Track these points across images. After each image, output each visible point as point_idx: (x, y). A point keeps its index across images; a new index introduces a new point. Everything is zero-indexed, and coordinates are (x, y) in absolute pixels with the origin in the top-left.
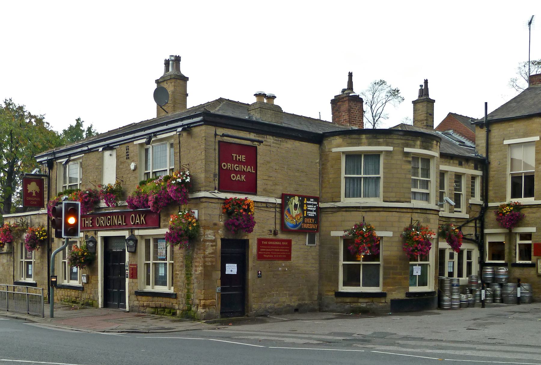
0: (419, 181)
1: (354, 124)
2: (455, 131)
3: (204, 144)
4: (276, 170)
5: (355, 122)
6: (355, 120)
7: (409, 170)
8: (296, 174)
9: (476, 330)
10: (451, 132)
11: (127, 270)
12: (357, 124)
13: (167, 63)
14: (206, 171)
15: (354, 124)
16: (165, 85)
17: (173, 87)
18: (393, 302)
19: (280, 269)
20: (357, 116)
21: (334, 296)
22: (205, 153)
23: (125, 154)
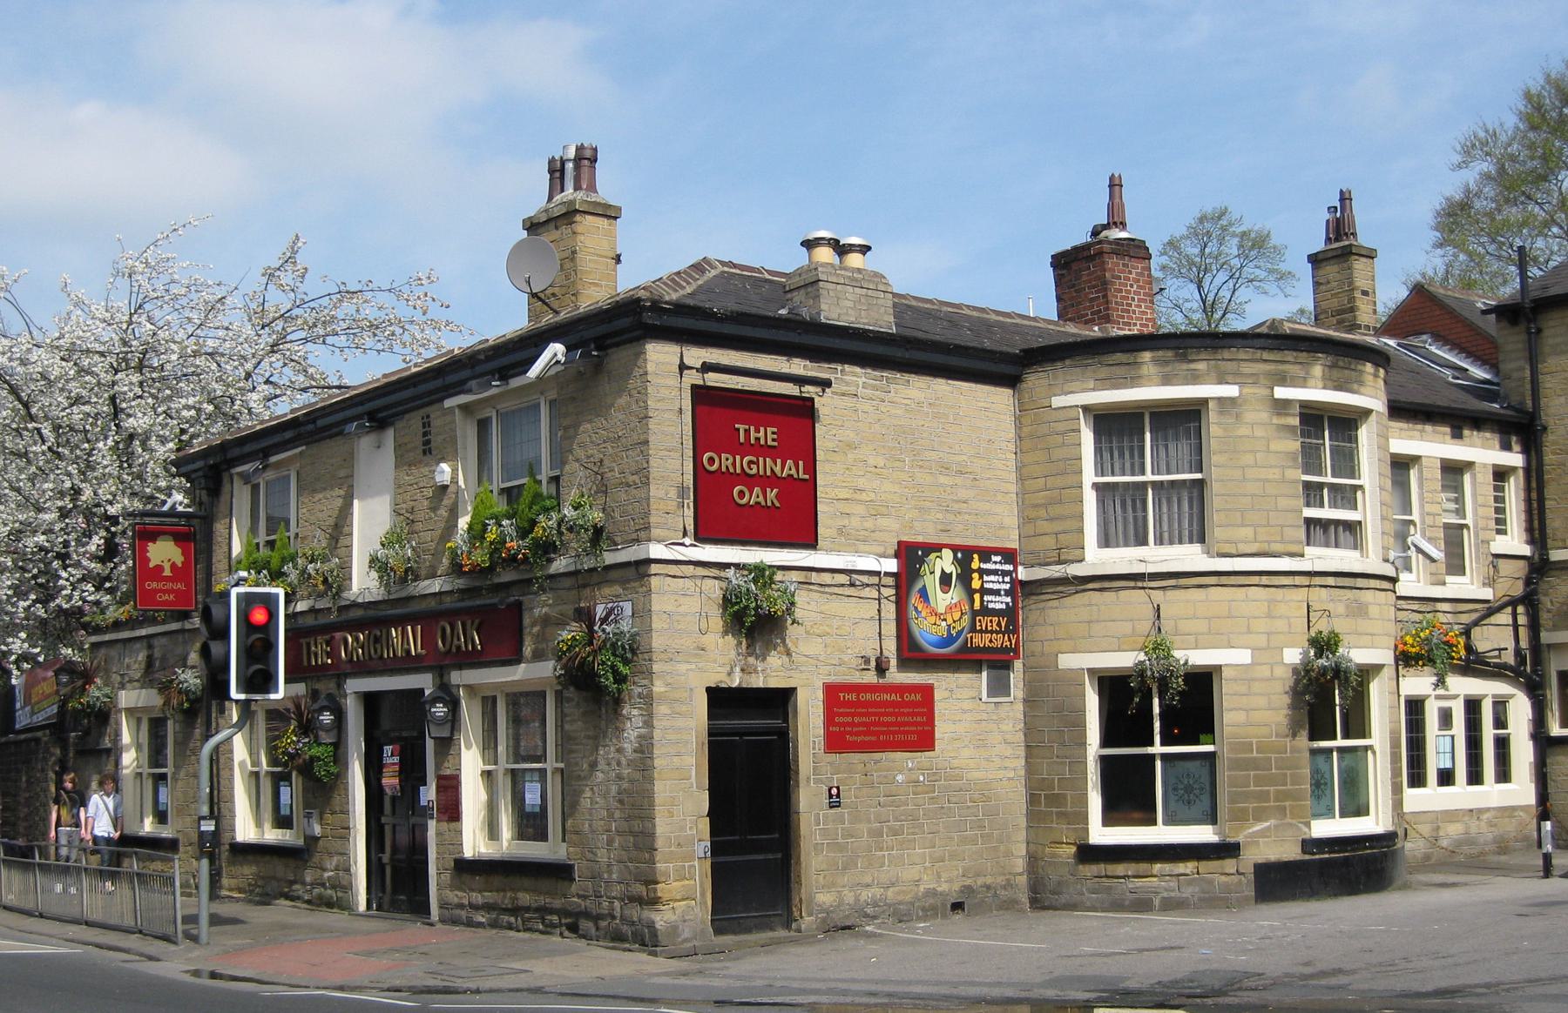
8: (942, 479)
15: (1124, 323)
20: (1133, 299)
23: (419, 440)
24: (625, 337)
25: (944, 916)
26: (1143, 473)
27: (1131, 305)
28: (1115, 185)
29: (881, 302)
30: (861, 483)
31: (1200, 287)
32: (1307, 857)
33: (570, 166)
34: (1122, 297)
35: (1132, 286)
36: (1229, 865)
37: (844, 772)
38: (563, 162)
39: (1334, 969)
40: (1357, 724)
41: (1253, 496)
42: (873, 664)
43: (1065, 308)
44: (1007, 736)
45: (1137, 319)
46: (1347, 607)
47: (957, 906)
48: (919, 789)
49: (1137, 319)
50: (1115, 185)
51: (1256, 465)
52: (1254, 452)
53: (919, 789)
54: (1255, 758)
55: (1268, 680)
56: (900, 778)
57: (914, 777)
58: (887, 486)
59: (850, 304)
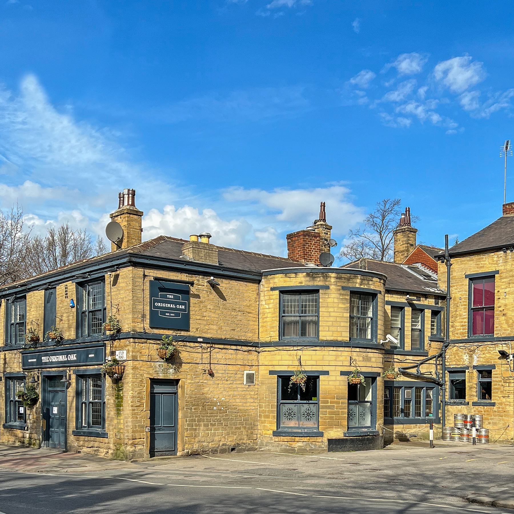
0: (393, 318)
1: (309, 259)
2: (423, 264)
3: (131, 285)
4: (211, 310)
5: (311, 257)
6: (311, 255)
7: (346, 309)
8: (233, 313)
9: (108, 469)
10: (419, 265)
11: (447, 396)
12: (313, 260)
13: (121, 197)
14: (133, 312)
15: (309, 259)
16: (118, 220)
17: (126, 222)
18: (330, 441)
19: (215, 408)
20: (313, 251)
21: (272, 436)
22: (133, 294)
23: (64, 293)
24: (125, 265)
25: (229, 452)
26: (291, 313)
27: (312, 253)
28: (323, 205)
29: (214, 255)
30: (205, 314)
31: (381, 234)
32: (345, 438)
33: (126, 196)
34: (309, 250)
35: (313, 246)
36: (319, 439)
37: (196, 406)
38: (124, 195)
39: (122, 398)
40: (430, 404)
41: (332, 321)
42: (207, 372)
43: (290, 253)
44: (252, 396)
45: (314, 258)
46: (363, 358)
47: (233, 449)
48: (221, 412)
49: (314, 258)
50: (323, 205)
51: (334, 312)
52: (334, 307)
53: (221, 412)
54: (329, 405)
55: (335, 381)
56: (215, 408)
57: (220, 408)
58: (213, 315)
59: (203, 255)
